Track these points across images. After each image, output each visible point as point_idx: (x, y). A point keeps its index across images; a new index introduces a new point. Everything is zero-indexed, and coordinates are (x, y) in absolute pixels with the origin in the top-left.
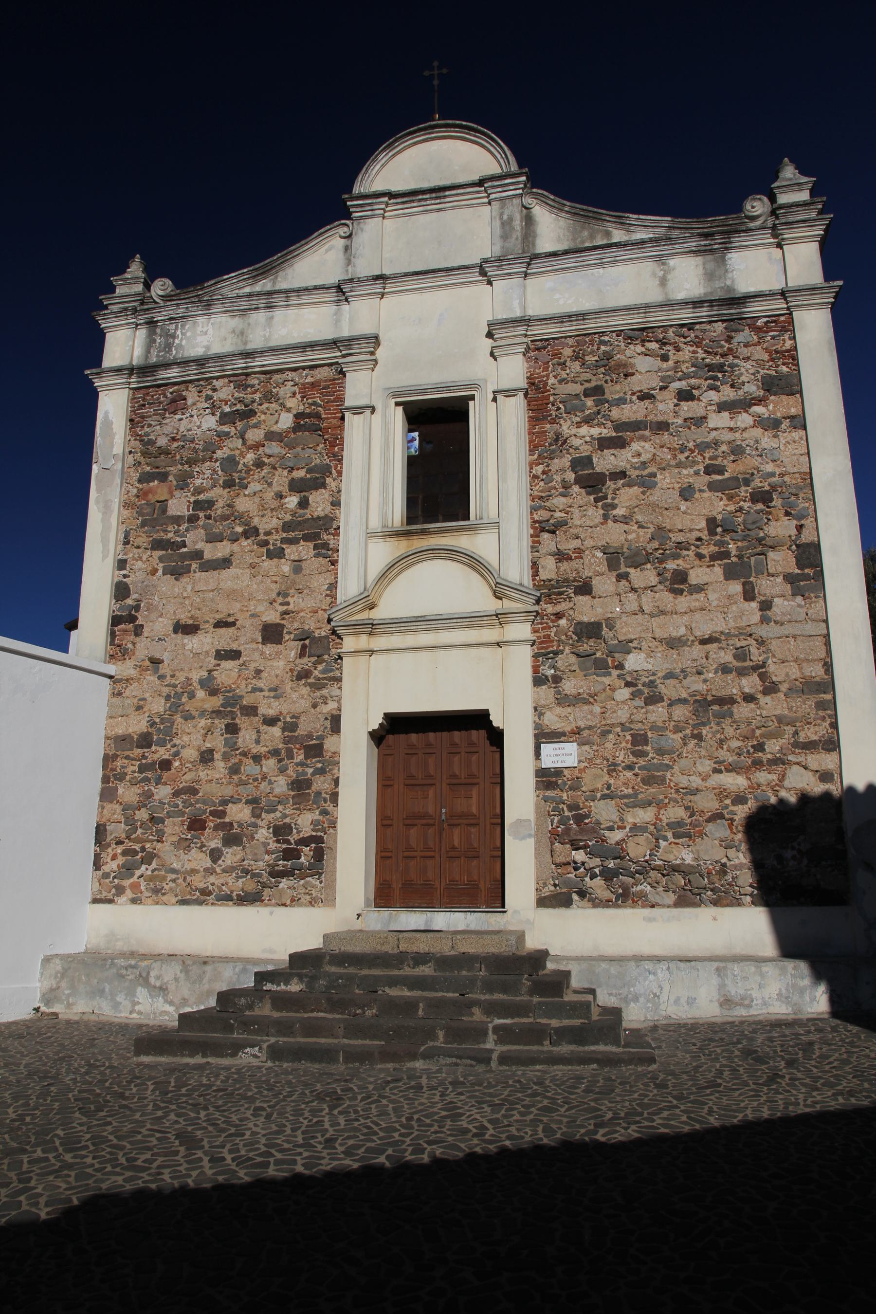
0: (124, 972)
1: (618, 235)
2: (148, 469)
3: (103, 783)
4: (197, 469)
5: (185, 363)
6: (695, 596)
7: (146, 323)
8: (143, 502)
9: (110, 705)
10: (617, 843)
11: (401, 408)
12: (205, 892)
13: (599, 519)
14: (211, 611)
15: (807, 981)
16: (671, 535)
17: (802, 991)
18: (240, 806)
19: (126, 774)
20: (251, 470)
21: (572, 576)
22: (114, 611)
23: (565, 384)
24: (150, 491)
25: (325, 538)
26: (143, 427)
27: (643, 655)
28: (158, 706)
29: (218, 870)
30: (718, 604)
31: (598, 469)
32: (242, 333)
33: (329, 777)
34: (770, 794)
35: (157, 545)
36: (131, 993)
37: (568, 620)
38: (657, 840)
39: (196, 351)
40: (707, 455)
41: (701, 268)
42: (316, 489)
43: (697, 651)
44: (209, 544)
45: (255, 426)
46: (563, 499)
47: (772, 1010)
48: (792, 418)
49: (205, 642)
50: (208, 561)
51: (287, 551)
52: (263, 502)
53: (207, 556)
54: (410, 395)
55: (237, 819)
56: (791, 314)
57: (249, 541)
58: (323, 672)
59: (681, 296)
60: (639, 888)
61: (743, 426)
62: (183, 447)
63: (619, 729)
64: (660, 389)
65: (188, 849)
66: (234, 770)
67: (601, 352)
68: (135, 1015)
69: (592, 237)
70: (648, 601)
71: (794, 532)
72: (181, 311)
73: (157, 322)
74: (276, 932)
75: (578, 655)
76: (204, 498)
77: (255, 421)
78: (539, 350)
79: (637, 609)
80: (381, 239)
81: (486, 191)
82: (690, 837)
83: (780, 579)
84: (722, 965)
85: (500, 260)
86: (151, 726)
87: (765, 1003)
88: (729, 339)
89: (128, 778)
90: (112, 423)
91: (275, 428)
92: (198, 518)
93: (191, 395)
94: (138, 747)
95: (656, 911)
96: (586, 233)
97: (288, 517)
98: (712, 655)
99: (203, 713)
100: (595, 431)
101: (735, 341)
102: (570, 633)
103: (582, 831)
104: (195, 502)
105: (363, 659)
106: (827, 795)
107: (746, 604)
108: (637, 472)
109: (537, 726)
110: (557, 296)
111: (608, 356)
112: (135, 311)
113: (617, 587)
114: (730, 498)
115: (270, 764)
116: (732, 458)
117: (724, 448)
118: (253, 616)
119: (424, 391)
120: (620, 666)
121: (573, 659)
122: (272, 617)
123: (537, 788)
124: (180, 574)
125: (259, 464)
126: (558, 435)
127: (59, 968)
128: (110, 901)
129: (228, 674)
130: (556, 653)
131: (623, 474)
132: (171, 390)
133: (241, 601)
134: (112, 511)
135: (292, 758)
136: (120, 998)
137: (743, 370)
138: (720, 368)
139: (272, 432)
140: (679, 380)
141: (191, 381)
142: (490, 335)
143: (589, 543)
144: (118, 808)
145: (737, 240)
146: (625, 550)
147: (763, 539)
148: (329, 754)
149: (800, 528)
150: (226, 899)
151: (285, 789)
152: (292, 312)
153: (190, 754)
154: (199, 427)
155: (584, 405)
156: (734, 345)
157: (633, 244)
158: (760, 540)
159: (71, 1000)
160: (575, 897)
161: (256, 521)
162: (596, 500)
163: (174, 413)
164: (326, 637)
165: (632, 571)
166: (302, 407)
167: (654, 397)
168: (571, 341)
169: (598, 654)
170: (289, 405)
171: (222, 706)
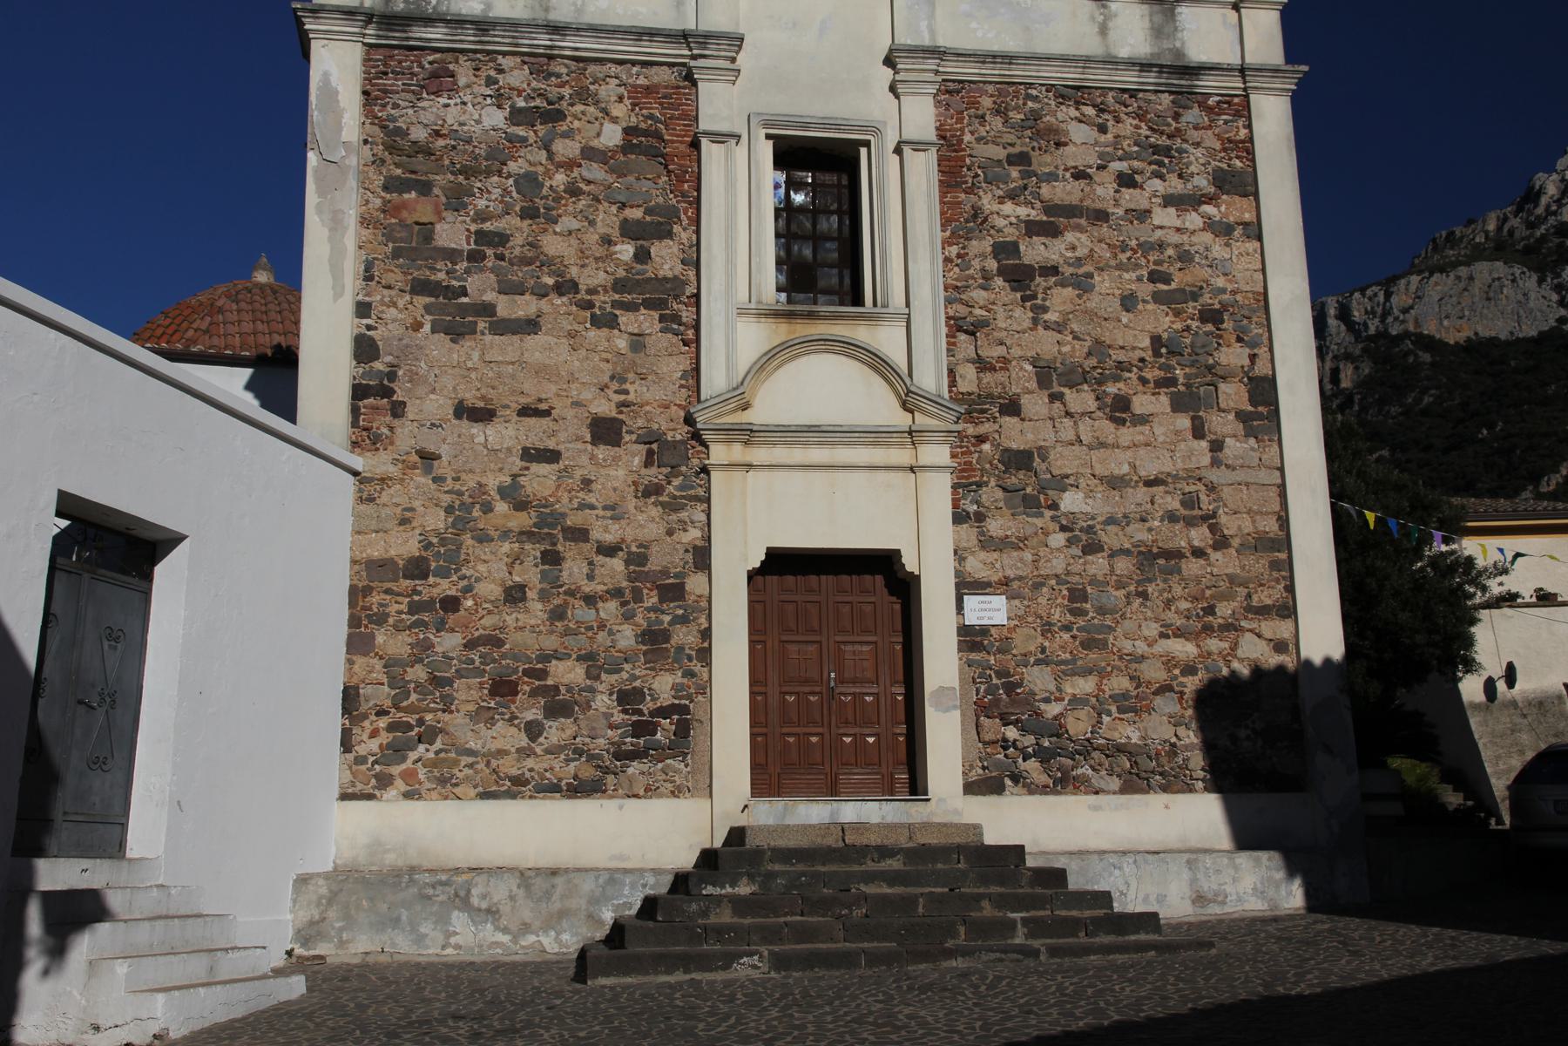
0: (430, 891)
3: (350, 626)
4: (479, 185)
6: (1139, 428)
9: (357, 516)
10: (1055, 718)
12: (519, 781)
13: (1027, 324)
15: (1280, 875)
17: (1277, 887)
18: (569, 663)
19: (388, 615)
21: (997, 391)
23: (987, 144)
27: (1081, 495)
28: (436, 520)
29: (538, 750)
30: (1162, 441)
33: (694, 628)
34: (1221, 664)
35: (420, 287)
36: (443, 920)
38: (1099, 715)
40: (1151, 258)
41: (1147, 19)
43: (1142, 494)
44: (502, 297)
45: (566, 135)
47: (1248, 907)
48: (1246, 224)
49: (506, 434)
50: (504, 320)
52: (581, 242)
54: (786, 127)
55: (565, 680)
56: (1247, 96)
57: (564, 299)
58: (681, 488)
59: (1123, 53)
60: (1080, 771)
61: (1191, 227)
62: (454, 147)
63: (1053, 582)
65: (491, 722)
66: (558, 614)
68: (449, 951)
70: (1086, 430)
71: (1247, 362)
74: (648, 835)
75: (1005, 490)
78: (951, 93)
82: (1136, 712)
83: (1231, 417)
84: (1193, 856)
86: (426, 548)
87: (1239, 900)
88: (1177, 117)
89: (391, 621)
90: (337, 93)
91: (595, 143)
92: (484, 257)
94: (405, 577)
95: (1101, 797)
97: (621, 273)
98: (1158, 500)
99: (506, 534)
100: (1023, 211)
101: (1183, 119)
103: (1013, 702)
105: (738, 475)
106: (1281, 669)
108: (1071, 270)
109: (958, 573)
111: (1036, 116)
114: (1177, 314)
115: (610, 608)
116: (1179, 265)
117: (1170, 252)
119: (805, 126)
120: (1054, 506)
121: (1000, 494)
123: (960, 650)
124: (461, 335)
125: (573, 191)
126: (976, 212)
127: (324, 891)
128: (370, 797)
129: (540, 481)
130: (979, 485)
131: (1053, 270)
132: (430, 58)
135: (642, 601)
136: (425, 928)
137: (1192, 158)
138: (1167, 152)
140: (1120, 159)
141: (462, 51)
142: (889, 62)
144: (378, 665)
147: (1213, 367)
148: (693, 597)
149: (1253, 357)
150: (551, 789)
151: (632, 642)
153: (490, 590)
154: (478, 122)
155: (1008, 175)
156: (1182, 126)
158: (1210, 368)
159: (345, 936)
160: (1008, 782)
161: (574, 272)
162: (1024, 299)
163: (437, 93)
164: (683, 442)
165: (1066, 391)
168: (990, 89)
169: (1029, 490)
170: (615, 113)
171: (535, 525)
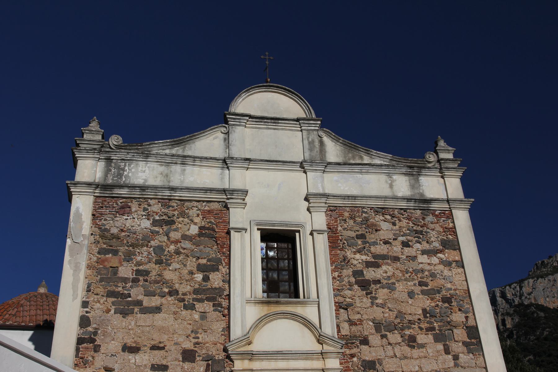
1: (366, 160)
2: (105, 246)
4: (138, 251)
5: (133, 187)
6: (421, 350)
7: (105, 159)
8: (101, 266)
11: (259, 231)
13: (369, 304)
14: (148, 339)
16: (406, 316)
20: (173, 255)
22: (79, 335)
23: (348, 231)
24: (106, 260)
25: (220, 300)
26: (101, 220)
31: (367, 278)
32: (167, 176)
35: (111, 294)
37: (358, 358)
39: (139, 181)
41: (408, 182)
42: (214, 271)
44: (146, 297)
45: (176, 230)
46: (350, 292)
48: (456, 261)
50: (146, 307)
51: (197, 306)
52: (180, 274)
53: (145, 304)
56: (451, 211)
57: (172, 298)
59: (400, 194)
61: (434, 263)
62: (129, 236)
64: (393, 240)
67: (363, 216)
69: (354, 158)
70: (397, 349)
71: (464, 320)
72: (129, 157)
73: (113, 159)
76: (143, 268)
77: (175, 227)
78: (333, 211)
79: (393, 355)
80: (246, 139)
81: (300, 125)
83: (461, 344)
85: (312, 162)
88: (424, 219)
90: (82, 215)
91: (187, 233)
92: (139, 281)
93: (134, 206)
96: (350, 155)
97: (197, 286)
100: (364, 257)
101: (426, 220)
102: (360, 366)
104: (136, 270)
107: (446, 356)
108: (386, 281)
110: (340, 185)
111: (367, 219)
112: (100, 152)
113: (382, 342)
114: (432, 299)
116: (431, 279)
117: (427, 273)
118: (176, 344)
119: (273, 225)
122: (188, 345)
124: (127, 314)
125: (178, 253)
131: (379, 282)
132: (121, 201)
133: (168, 334)
134: (81, 270)
137: (432, 235)
138: (421, 232)
139: (186, 235)
142: (306, 199)
143: (365, 317)
145: (424, 171)
146: (384, 322)
149: (467, 318)
152: (196, 169)
155: (357, 243)
156: (426, 222)
157: (377, 166)
158: (449, 323)
161: (177, 286)
162: (367, 294)
163: (123, 215)
164: (222, 360)
165: (388, 333)
166: (203, 223)
167: (391, 244)
168: (348, 209)
